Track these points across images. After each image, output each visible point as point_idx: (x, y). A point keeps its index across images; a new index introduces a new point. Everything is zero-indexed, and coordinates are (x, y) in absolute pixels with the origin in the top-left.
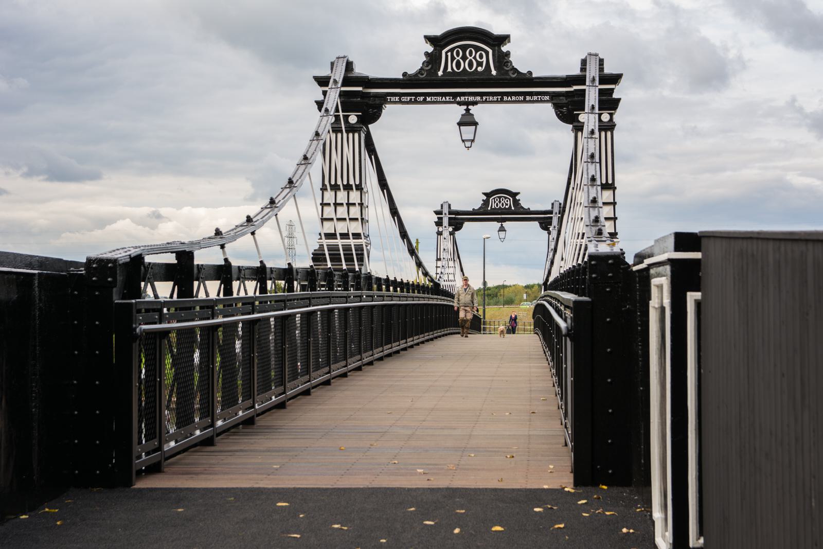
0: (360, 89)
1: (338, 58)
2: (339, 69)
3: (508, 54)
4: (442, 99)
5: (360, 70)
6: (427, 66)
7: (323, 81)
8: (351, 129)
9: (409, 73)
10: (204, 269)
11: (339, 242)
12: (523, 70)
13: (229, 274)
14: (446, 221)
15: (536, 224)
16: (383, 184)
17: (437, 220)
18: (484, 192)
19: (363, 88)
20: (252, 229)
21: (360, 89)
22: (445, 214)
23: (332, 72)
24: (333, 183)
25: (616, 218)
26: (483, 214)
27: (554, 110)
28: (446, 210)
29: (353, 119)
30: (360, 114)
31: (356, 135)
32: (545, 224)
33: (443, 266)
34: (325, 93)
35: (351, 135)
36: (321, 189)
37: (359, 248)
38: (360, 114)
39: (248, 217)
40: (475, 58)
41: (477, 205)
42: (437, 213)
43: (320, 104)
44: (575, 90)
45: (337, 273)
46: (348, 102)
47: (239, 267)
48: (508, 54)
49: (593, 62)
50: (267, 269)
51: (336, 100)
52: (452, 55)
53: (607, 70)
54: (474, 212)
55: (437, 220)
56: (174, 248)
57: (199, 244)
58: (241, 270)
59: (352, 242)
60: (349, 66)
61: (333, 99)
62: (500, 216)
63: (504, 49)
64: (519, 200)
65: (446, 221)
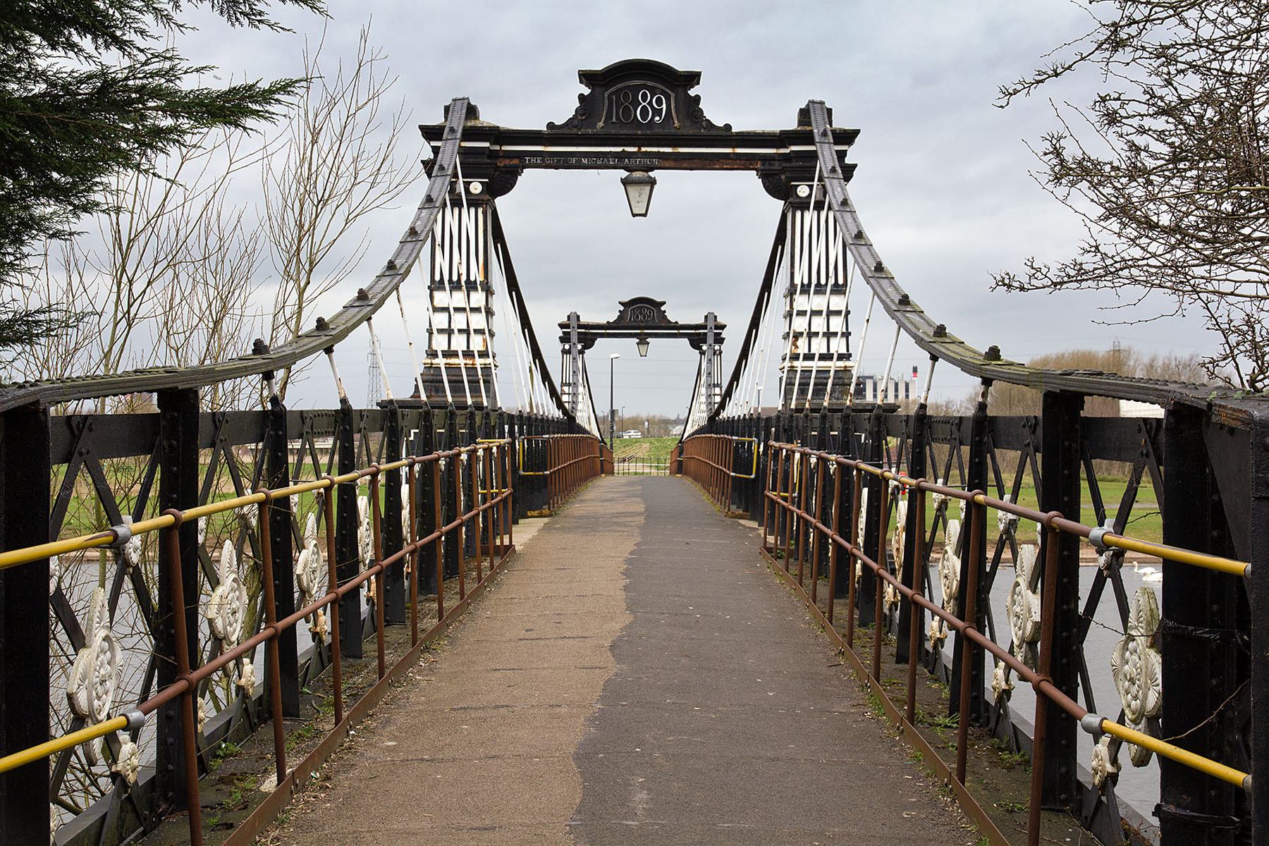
0: (487, 144)
1: (454, 100)
2: (456, 115)
3: (697, 99)
4: (603, 161)
5: (489, 117)
6: (582, 115)
7: (431, 133)
8: (474, 202)
9: (558, 123)
10: (227, 422)
11: (461, 361)
12: (719, 123)
13: (173, 628)
14: (574, 338)
15: (686, 341)
16: (513, 285)
17: (561, 335)
18: (621, 300)
19: (491, 144)
20: (993, 366)
21: (487, 144)
22: (573, 327)
23: (446, 118)
24: (455, 278)
25: (850, 334)
26: (614, 329)
27: (760, 180)
28: (574, 323)
29: (476, 188)
30: (487, 180)
31: (480, 210)
32: (697, 341)
33: (574, 394)
34: (436, 150)
35: (472, 210)
36: (429, 287)
37: (486, 369)
38: (487, 180)
39: (320, 321)
40: (650, 103)
41: (613, 317)
42: (562, 326)
43: (429, 166)
44: (786, 147)
45: (459, 412)
46: (472, 164)
47: (302, 412)
48: (697, 99)
49: (818, 112)
50: (354, 413)
51: (454, 157)
52: (618, 99)
53: (837, 124)
54: (609, 326)
55: (561, 335)
56: (162, 381)
57: (215, 376)
58: (306, 418)
59: (479, 362)
60: (472, 111)
61: (450, 155)
62: (693, 331)
63: (692, 92)
64: (665, 311)
65: (574, 338)
